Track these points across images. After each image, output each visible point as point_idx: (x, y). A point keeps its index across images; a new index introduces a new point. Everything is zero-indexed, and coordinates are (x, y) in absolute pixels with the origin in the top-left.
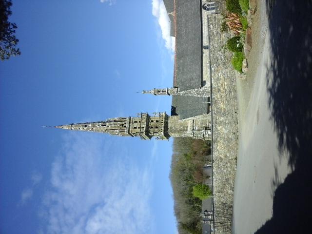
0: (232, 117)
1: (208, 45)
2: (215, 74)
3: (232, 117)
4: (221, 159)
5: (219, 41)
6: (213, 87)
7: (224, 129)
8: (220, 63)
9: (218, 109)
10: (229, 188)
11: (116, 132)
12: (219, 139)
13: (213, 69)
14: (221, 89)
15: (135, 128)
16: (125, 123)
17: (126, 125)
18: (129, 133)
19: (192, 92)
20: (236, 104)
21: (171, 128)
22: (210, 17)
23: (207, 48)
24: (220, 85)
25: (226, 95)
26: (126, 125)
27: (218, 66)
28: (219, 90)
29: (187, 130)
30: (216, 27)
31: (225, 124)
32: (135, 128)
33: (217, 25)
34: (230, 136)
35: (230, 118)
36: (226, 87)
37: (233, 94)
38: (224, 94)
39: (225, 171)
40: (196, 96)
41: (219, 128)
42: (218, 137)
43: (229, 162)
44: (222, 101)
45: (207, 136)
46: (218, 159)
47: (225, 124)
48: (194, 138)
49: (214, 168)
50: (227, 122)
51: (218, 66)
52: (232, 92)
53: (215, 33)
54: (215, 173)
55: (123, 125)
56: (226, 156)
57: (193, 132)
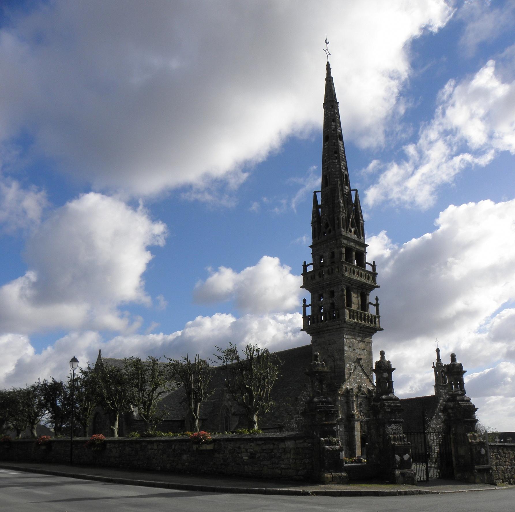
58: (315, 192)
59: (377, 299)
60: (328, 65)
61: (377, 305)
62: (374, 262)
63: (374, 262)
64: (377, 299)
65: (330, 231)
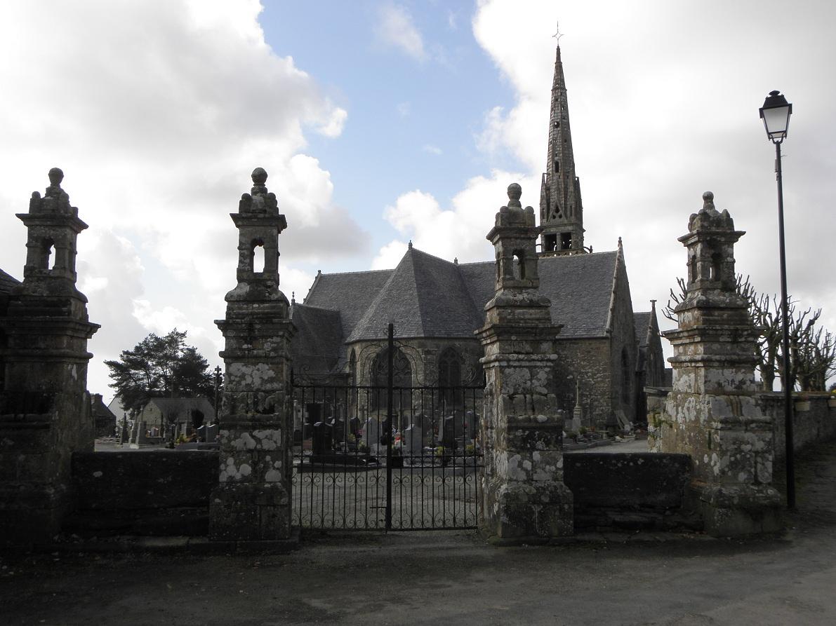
58: (544, 174)
60: (558, 49)
62: (591, 247)
63: (591, 247)
65: (560, 217)
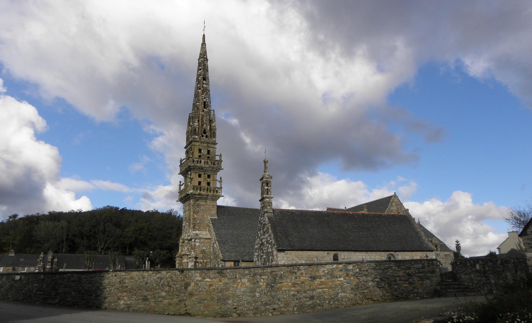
0: (266, 304)
1: (340, 260)
2: (341, 270)
3: (266, 304)
4: (187, 285)
5: (398, 279)
6: (319, 267)
7: (243, 289)
8: (361, 279)
9: (281, 277)
10: (129, 302)
11: (194, 122)
12: (225, 280)
13: (350, 267)
14: (317, 281)
15: (200, 150)
16: (207, 137)
17: (204, 137)
18: (191, 142)
19: (267, 235)
20: (291, 310)
21: (199, 206)
22: (433, 264)
23: (336, 258)
24: (323, 280)
25: (305, 292)
26: (204, 137)
27: (355, 275)
28: (313, 278)
29: (194, 229)
30: (419, 272)
31: (253, 291)
32: (200, 150)
33: (422, 274)
34: (230, 302)
35: (265, 299)
36: (320, 290)
37: (308, 303)
38: (307, 287)
39: (164, 294)
40: (258, 241)
41: (245, 280)
42: (229, 279)
43: (180, 301)
44: (294, 285)
45: (185, 260)
46: (187, 280)
47: (253, 291)
48: (181, 241)
49: (169, 274)
50: (257, 294)
51: (355, 275)
52: (311, 302)
53: (410, 271)
54: (159, 275)
55: (205, 132)
56: (191, 294)
57: (191, 240)
59: (221, 178)
61: (220, 182)
64: (221, 178)
